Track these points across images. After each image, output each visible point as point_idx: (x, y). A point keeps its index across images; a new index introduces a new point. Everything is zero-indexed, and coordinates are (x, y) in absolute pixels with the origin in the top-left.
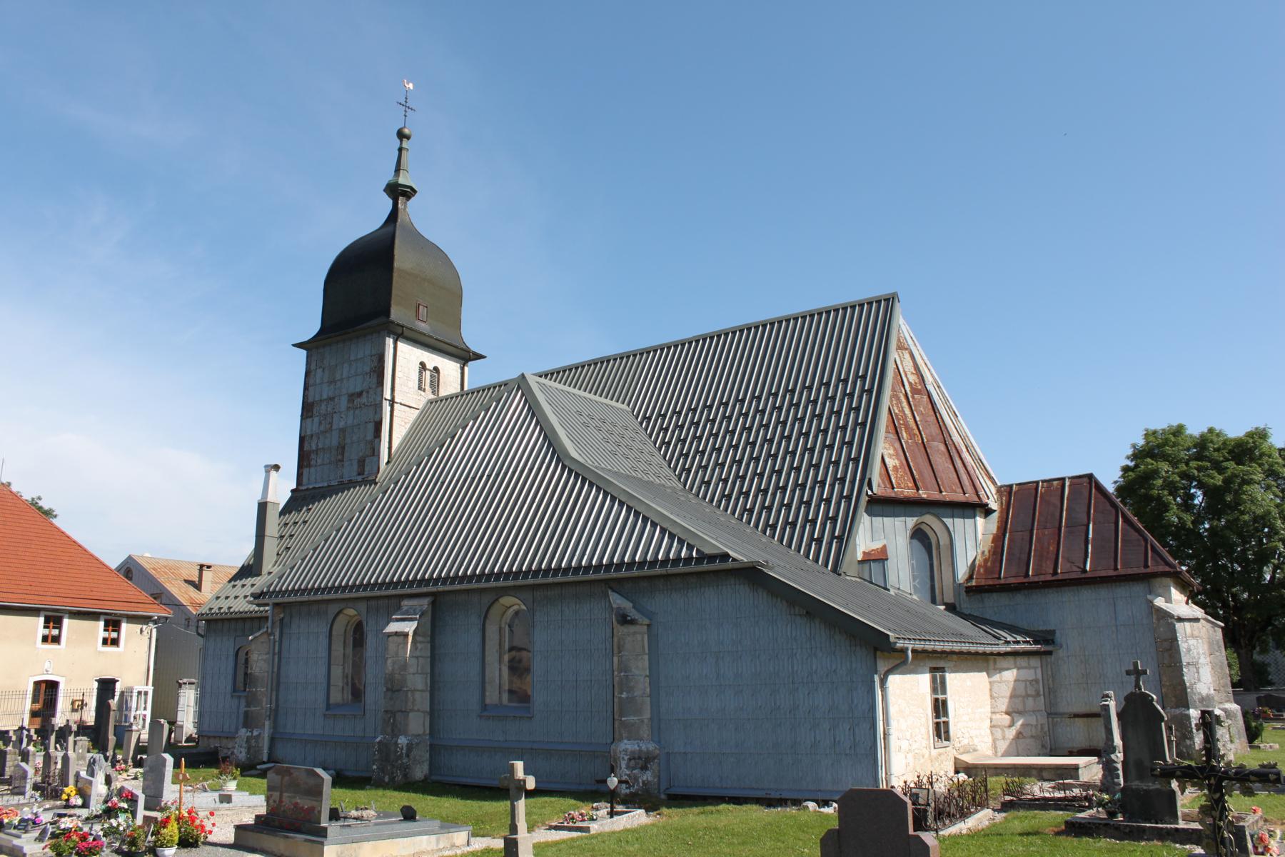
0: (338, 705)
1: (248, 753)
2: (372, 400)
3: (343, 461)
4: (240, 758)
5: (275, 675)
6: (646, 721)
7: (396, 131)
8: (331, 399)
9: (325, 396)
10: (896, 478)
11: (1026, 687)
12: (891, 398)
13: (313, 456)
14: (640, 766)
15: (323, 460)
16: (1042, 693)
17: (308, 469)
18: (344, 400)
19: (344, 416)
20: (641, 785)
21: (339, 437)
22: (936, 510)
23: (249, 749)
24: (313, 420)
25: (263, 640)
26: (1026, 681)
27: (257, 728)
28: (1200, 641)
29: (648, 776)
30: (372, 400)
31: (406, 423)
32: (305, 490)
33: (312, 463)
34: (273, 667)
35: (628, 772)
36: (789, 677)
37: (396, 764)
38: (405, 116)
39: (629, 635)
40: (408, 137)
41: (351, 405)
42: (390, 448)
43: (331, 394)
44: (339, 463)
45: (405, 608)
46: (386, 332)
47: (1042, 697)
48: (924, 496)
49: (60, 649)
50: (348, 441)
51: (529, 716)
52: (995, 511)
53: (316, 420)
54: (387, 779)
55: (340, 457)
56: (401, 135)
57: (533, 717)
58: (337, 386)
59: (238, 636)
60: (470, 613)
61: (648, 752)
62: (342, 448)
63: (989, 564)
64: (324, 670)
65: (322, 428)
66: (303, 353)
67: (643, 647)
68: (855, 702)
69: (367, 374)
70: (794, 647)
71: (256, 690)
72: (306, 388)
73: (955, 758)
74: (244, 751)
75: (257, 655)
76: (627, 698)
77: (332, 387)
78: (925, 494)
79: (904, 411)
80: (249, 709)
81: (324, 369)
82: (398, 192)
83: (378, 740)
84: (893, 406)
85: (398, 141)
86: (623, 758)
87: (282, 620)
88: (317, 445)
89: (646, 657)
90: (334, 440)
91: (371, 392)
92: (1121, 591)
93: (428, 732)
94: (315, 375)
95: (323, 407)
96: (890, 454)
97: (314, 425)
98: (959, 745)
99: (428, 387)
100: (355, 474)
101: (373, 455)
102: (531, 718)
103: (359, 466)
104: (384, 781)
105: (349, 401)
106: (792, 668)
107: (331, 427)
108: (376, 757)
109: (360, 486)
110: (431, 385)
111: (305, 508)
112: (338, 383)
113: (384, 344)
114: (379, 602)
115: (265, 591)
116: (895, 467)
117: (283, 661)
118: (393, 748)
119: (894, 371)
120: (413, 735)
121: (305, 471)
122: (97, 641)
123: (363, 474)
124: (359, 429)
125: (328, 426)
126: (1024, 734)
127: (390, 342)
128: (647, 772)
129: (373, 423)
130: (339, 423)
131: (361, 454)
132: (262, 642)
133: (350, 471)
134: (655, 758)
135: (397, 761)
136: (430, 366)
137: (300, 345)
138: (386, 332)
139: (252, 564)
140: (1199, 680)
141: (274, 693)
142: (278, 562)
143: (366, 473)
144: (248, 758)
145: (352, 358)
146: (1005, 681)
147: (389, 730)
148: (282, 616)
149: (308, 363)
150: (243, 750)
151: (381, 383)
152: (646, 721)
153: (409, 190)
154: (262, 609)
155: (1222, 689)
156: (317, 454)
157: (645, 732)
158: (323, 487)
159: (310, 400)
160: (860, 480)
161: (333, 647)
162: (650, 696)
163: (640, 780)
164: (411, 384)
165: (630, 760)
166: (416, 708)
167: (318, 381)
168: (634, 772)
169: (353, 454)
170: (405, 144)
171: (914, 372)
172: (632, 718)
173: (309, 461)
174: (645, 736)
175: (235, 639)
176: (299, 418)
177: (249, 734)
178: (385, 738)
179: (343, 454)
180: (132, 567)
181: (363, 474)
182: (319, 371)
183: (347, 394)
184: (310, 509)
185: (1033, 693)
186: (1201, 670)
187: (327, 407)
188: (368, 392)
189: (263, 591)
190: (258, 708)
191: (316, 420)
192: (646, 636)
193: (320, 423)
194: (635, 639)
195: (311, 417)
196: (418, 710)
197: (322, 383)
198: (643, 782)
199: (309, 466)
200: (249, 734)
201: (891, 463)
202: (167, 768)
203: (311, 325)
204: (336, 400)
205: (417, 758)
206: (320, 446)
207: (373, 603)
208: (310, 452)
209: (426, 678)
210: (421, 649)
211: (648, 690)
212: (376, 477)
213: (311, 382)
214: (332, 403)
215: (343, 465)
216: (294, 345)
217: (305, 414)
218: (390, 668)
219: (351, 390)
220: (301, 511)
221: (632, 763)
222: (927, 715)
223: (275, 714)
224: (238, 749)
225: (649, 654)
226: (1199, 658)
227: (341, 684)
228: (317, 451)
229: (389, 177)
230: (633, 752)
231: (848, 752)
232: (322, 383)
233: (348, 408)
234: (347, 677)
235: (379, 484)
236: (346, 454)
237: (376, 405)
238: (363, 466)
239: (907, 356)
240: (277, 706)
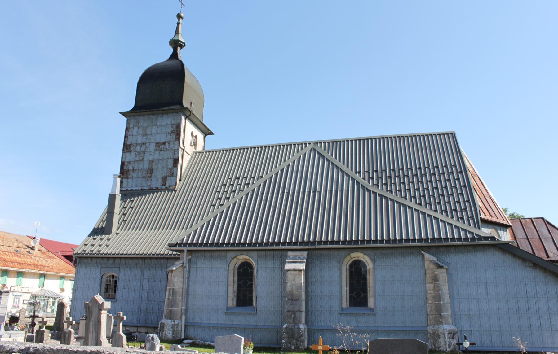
0: (231, 308)
1: (173, 334)
4: (169, 336)
6: (450, 315)
7: (177, 14)
8: (143, 144)
13: (130, 173)
14: (451, 337)
17: (126, 180)
18: (152, 147)
20: (453, 346)
21: (149, 164)
22: (496, 227)
23: (173, 331)
24: (131, 154)
25: (179, 270)
27: (176, 320)
32: (125, 190)
33: (129, 176)
36: (525, 295)
37: (300, 339)
38: (181, 8)
39: (440, 273)
40: (182, 18)
41: (158, 148)
43: (144, 141)
45: (291, 257)
46: (182, 113)
51: (373, 313)
54: (293, 348)
55: (149, 175)
56: (179, 17)
57: (376, 314)
58: (148, 138)
59: (103, 267)
60: (332, 261)
61: (454, 330)
65: (137, 158)
66: (125, 119)
71: (176, 299)
72: (126, 136)
74: (171, 332)
75: (176, 279)
80: (172, 309)
81: (139, 128)
82: (176, 44)
85: (177, 20)
86: (446, 333)
88: (133, 167)
89: (447, 284)
97: (130, 157)
101: (173, 175)
102: (375, 315)
103: (163, 181)
104: (291, 349)
105: (156, 146)
107: (144, 158)
109: (165, 191)
110: (194, 145)
111: (129, 200)
112: (149, 137)
113: (181, 119)
114: (220, 253)
115: (179, 242)
118: (297, 331)
123: (166, 185)
124: (163, 161)
125: (141, 158)
127: (183, 118)
128: (454, 340)
129: (173, 159)
130: (148, 157)
131: (164, 175)
132: (179, 272)
133: (156, 183)
134: (456, 333)
135: (300, 338)
136: (194, 135)
137: (124, 114)
138: (182, 113)
139: (104, 227)
142: (120, 228)
143: (167, 185)
144: (173, 337)
145: (159, 124)
147: (291, 321)
148: (190, 257)
149: (127, 123)
150: (170, 332)
151: (179, 139)
152: (450, 315)
153: (183, 44)
154: (174, 253)
156: (133, 172)
158: (138, 190)
160: (474, 211)
162: (450, 303)
163: (453, 344)
165: (448, 334)
168: (450, 340)
169: (159, 174)
170: (181, 20)
174: (450, 322)
175: (101, 269)
176: (121, 152)
177: (173, 323)
179: (151, 173)
183: (155, 142)
184: (133, 201)
187: (141, 148)
188: (169, 143)
189: (178, 242)
190: (177, 309)
192: (446, 274)
193: (136, 156)
199: (127, 177)
200: (173, 323)
202: (242, 341)
203: (130, 105)
204: (147, 145)
206: (136, 167)
207: (262, 253)
208: (127, 171)
211: (449, 300)
212: (175, 187)
214: (145, 146)
215: (151, 179)
216: (120, 113)
217: (125, 150)
218: (290, 288)
219: (158, 141)
220: (126, 201)
223: (186, 312)
224: (168, 332)
225: (448, 283)
227: (232, 297)
228: (133, 170)
229: (171, 36)
234: (235, 293)
235: (177, 191)
236: (153, 174)
237: (174, 150)
240: (187, 307)
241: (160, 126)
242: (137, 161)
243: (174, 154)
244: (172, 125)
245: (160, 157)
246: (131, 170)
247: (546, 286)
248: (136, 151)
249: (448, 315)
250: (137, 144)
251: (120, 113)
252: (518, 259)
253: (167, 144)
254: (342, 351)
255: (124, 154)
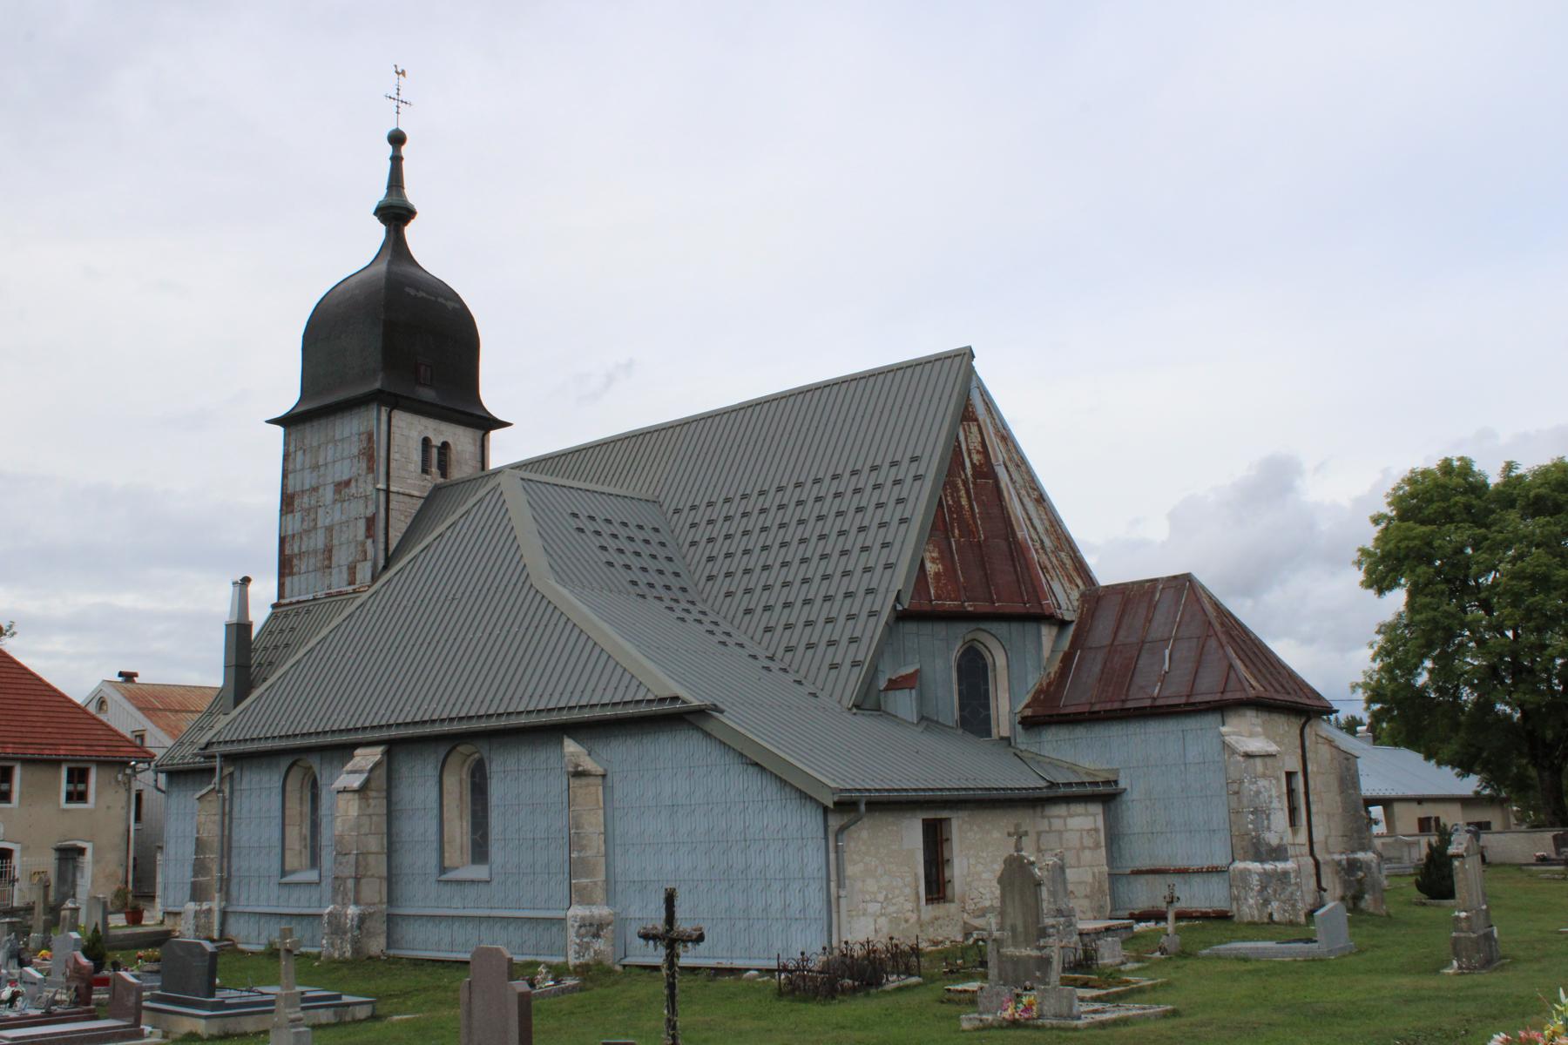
2: (362, 490)
3: (330, 567)
5: (225, 839)
6: (600, 883)
8: (315, 489)
9: (307, 486)
10: (937, 588)
11: (1081, 838)
12: (945, 485)
13: (295, 562)
15: (307, 565)
16: (1103, 843)
18: (328, 494)
19: (330, 512)
20: (592, 954)
21: (326, 538)
26: (1082, 830)
28: (1274, 782)
29: (599, 945)
30: (362, 490)
31: (406, 517)
33: (295, 570)
34: (223, 831)
35: (578, 941)
38: (398, 113)
41: (337, 497)
42: (387, 549)
43: (314, 483)
44: (326, 570)
47: (1103, 849)
48: (970, 609)
49: (11, 809)
50: (335, 542)
52: (1072, 622)
53: (298, 515)
55: (326, 563)
62: (329, 551)
63: (1052, 689)
64: (277, 834)
65: (305, 526)
66: (279, 431)
67: (598, 800)
68: (805, 860)
69: (355, 457)
70: (746, 799)
73: (965, 923)
76: (579, 858)
77: (315, 474)
78: (971, 606)
79: (960, 502)
81: (304, 451)
83: (327, 911)
84: (946, 496)
87: (231, 774)
88: (300, 547)
90: (319, 540)
91: (361, 479)
92: (1191, 724)
93: (385, 900)
94: (295, 459)
95: (306, 499)
96: (933, 558)
97: (295, 524)
98: (973, 907)
99: (434, 470)
100: (345, 583)
103: (349, 574)
106: (745, 822)
108: (326, 931)
112: (322, 469)
116: (937, 574)
117: (234, 824)
119: (954, 450)
120: (367, 904)
121: (288, 581)
122: (58, 795)
125: (312, 524)
126: (1076, 893)
131: (350, 559)
134: (608, 924)
136: (436, 441)
140: (1269, 828)
141: (226, 860)
143: (358, 582)
146: (1055, 831)
147: (339, 898)
149: (286, 444)
152: (600, 883)
155: (1355, 835)
157: (599, 894)
159: (290, 490)
161: (288, 805)
164: (412, 467)
165: (580, 927)
166: (369, 873)
167: (298, 467)
171: (981, 450)
172: (584, 881)
173: (292, 567)
178: (335, 908)
179: (330, 558)
180: (105, 696)
181: (354, 584)
182: (300, 453)
185: (1091, 845)
186: (1272, 817)
188: (357, 480)
191: (298, 515)
192: (601, 788)
193: (303, 520)
194: (591, 793)
195: (292, 512)
196: (372, 876)
197: (303, 469)
198: (595, 951)
199: (292, 574)
201: (931, 568)
203: (288, 397)
204: (321, 491)
205: (372, 930)
206: (304, 549)
209: (382, 839)
210: (375, 806)
213: (291, 467)
216: (269, 422)
219: (337, 479)
221: (583, 931)
222: (916, 874)
226: (1271, 802)
229: (379, 193)
230: (583, 918)
231: (798, 916)
232: (303, 469)
233: (335, 501)
234: (305, 839)
238: (355, 573)
239: (975, 429)
241: (340, 441)
242: (305, 531)
243: (366, 507)
244: (933, 923)
245: (344, 518)
246: (296, 555)
247: (1411, 875)
248: (302, 509)
249: (595, 883)
250: (303, 491)
251: (269, 422)
252: (701, 737)
253: (353, 484)
254: (5, 854)
255: (284, 518)
